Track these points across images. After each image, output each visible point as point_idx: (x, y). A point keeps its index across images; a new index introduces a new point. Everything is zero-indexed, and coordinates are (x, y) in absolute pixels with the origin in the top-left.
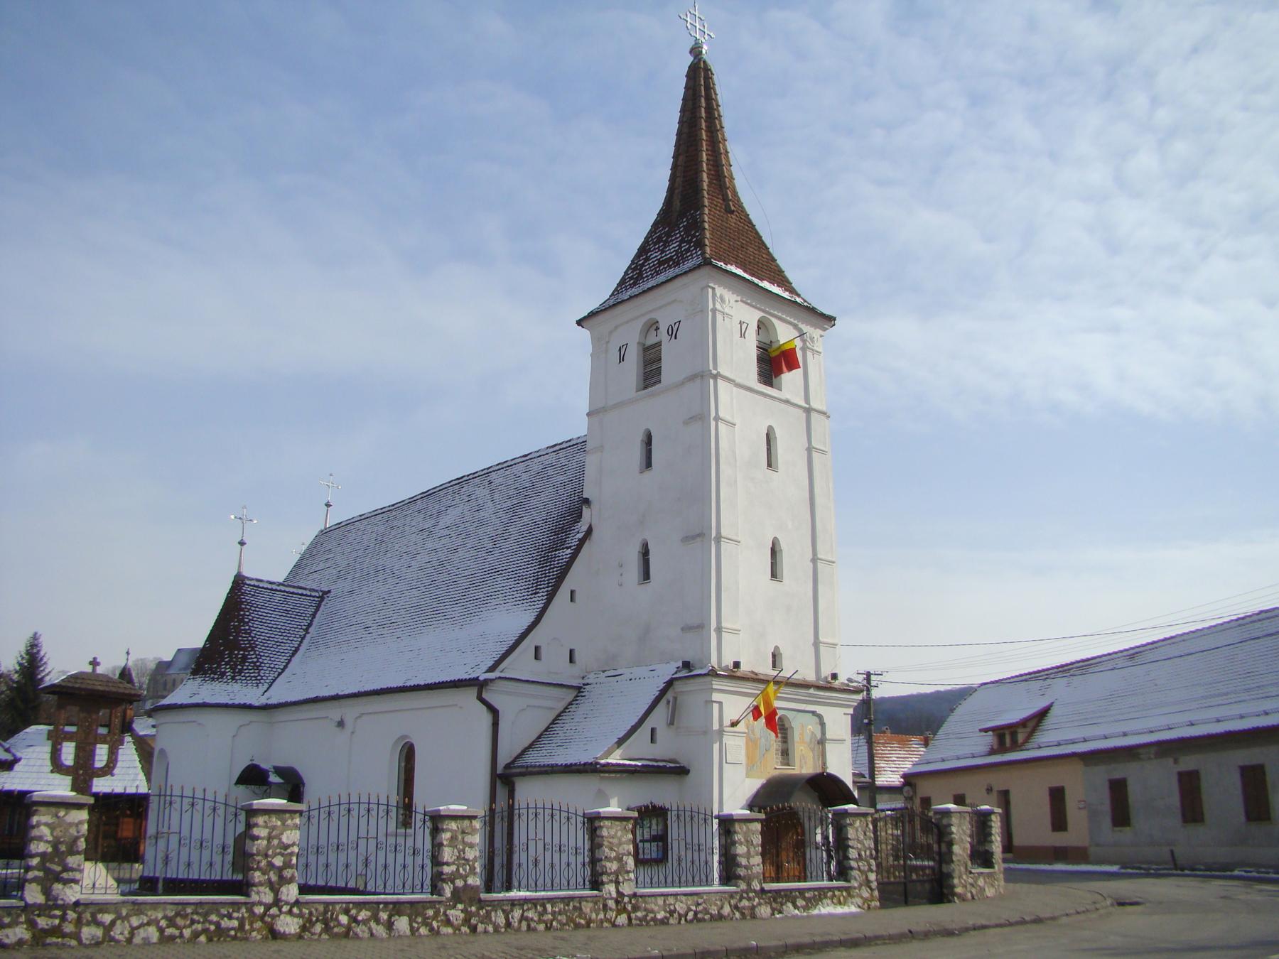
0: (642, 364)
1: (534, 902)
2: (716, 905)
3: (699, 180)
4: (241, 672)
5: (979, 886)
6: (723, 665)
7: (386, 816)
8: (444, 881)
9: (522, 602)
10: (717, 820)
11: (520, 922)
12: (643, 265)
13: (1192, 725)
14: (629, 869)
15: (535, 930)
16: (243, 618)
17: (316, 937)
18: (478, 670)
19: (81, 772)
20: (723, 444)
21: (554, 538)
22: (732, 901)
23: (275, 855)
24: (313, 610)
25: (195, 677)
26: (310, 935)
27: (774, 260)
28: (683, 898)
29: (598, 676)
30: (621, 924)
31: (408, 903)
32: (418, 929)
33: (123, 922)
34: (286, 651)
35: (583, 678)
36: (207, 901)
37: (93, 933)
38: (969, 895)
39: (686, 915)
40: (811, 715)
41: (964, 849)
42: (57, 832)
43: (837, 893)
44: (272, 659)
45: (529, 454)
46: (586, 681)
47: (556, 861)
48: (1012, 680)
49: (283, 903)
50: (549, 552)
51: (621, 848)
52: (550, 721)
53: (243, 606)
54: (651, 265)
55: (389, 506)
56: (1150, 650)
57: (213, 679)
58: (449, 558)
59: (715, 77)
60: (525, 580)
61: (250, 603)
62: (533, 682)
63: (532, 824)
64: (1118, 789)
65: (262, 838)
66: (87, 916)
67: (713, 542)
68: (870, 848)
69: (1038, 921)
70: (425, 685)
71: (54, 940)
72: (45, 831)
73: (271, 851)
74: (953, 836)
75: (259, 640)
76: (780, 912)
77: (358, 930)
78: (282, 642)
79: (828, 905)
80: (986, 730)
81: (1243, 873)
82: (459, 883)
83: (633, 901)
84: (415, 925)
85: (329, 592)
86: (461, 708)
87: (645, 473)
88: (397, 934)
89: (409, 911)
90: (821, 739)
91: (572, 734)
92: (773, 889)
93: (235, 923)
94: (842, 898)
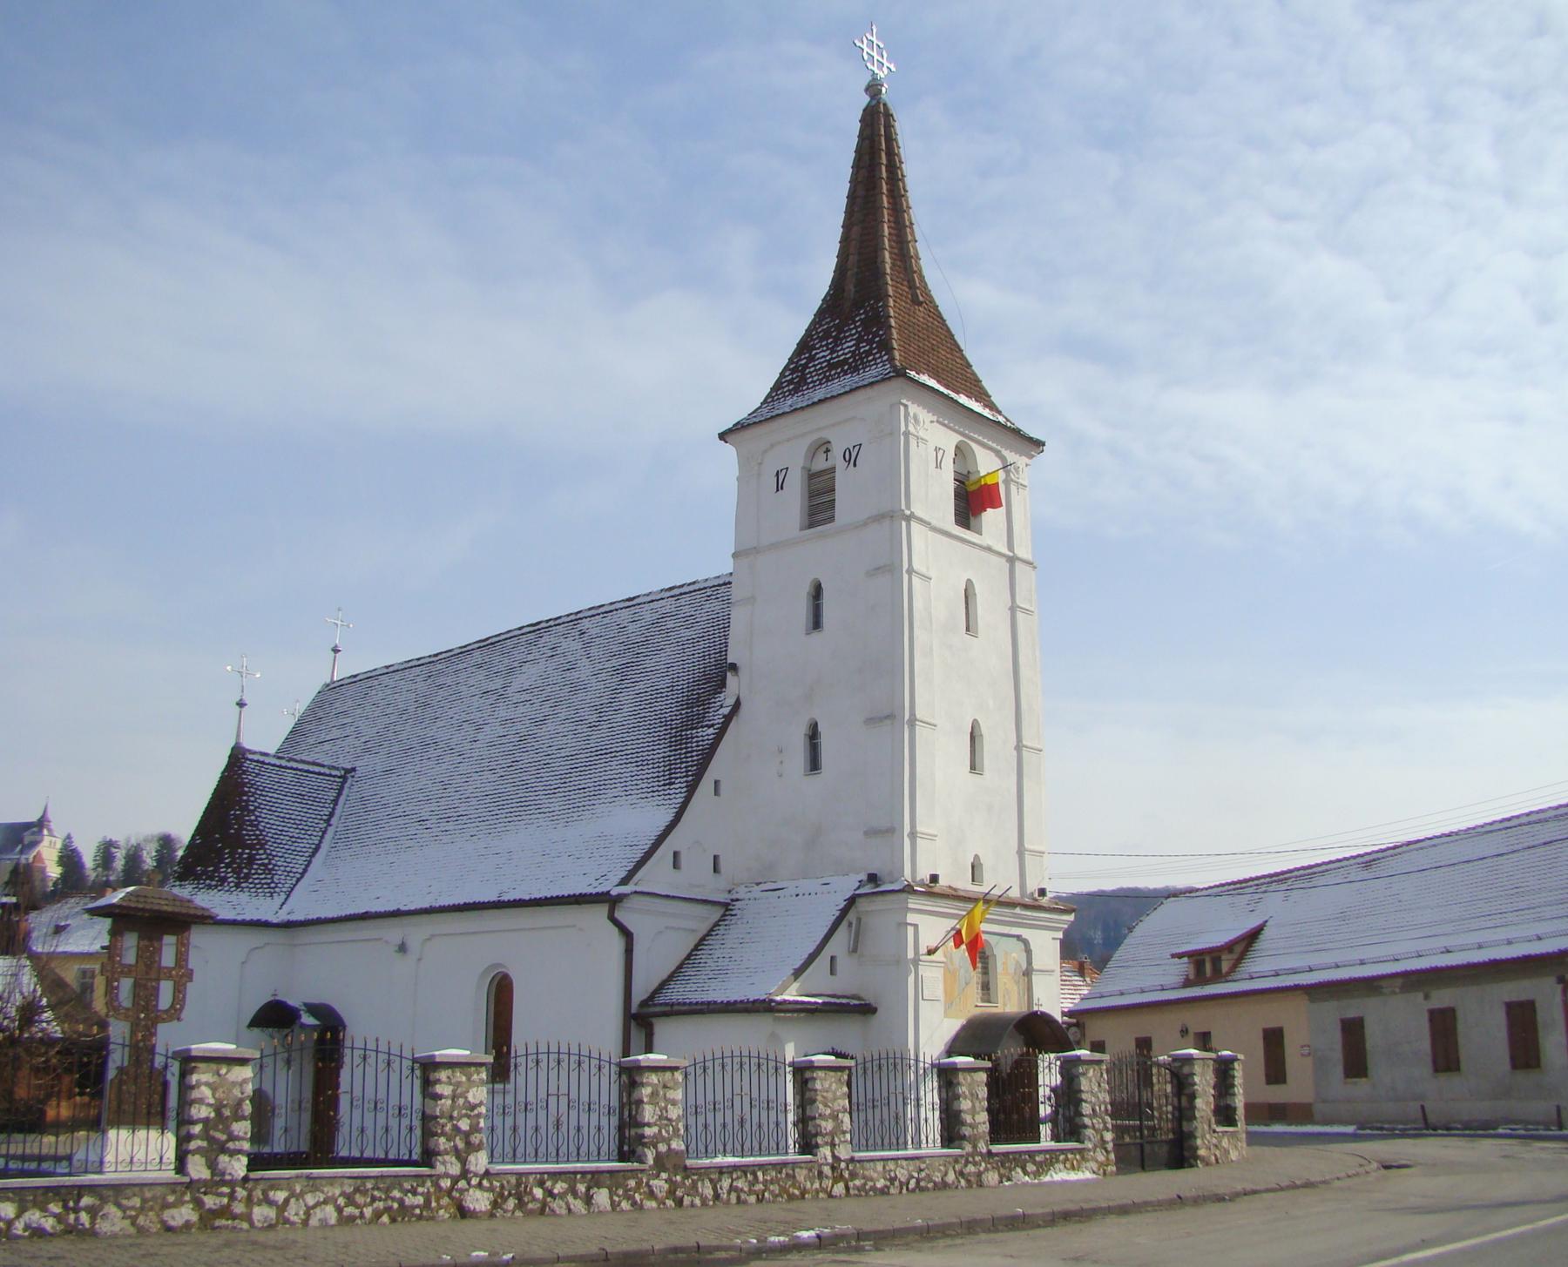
0: (807, 495)
1: (744, 1169)
2: (940, 1171)
3: (879, 260)
4: (247, 877)
6: (918, 879)
7: (557, 1068)
8: (645, 1145)
10: (791, 1068)
11: (729, 1193)
12: (806, 366)
13: (1448, 952)
14: (845, 1129)
15: (745, 1202)
16: (247, 805)
17: (509, 1214)
18: (606, 883)
19: (143, 1015)
21: (687, 713)
22: (956, 1166)
23: (461, 1117)
24: (335, 795)
25: (183, 883)
27: (969, 366)
28: (904, 1163)
29: (750, 889)
30: (838, 1195)
31: (608, 1172)
33: (297, 1200)
34: (304, 850)
35: (730, 892)
37: (265, 1213)
38: (1213, 1158)
39: (908, 1183)
40: (1015, 939)
41: (1207, 1103)
43: (1070, 1156)
46: (734, 897)
47: (584, 1123)
48: (1210, 891)
49: (472, 1175)
50: (682, 731)
51: (836, 1104)
52: (692, 946)
53: (246, 789)
54: (818, 367)
55: (430, 656)
57: (209, 887)
59: (897, 124)
61: (255, 784)
62: (674, 897)
63: (737, 1076)
64: (1353, 1031)
65: (446, 1097)
66: (258, 1193)
67: (906, 726)
68: (1104, 1102)
69: (1309, 1185)
70: (530, 900)
72: (206, 1092)
74: (1196, 1087)
75: (270, 835)
76: (1009, 1179)
77: (555, 1205)
78: (298, 838)
79: (1060, 1171)
80: (1180, 956)
81: (1509, 1131)
82: (662, 1148)
83: (850, 1168)
84: (616, 1199)
85: (354, 769)
86: (580, 929)
87: (813, 635)
88: (596, 1210)
89: (608, 1182)
90: (1027, 969)
91: (726, 963)
92: (1000, 1151)
94: (1075, 1162)
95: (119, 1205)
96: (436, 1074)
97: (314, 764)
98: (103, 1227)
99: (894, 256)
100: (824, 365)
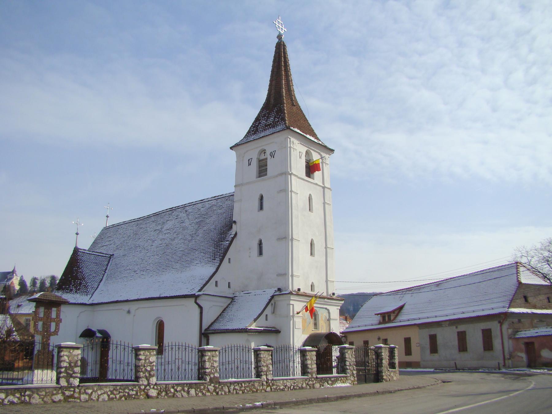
0: (258, 167)
1: (238, 383)
2: (301, 383)
3: (281, 92)
4: (79, 289)
5: (392, 376)
8: (206, 375)
9: (208, 263)
10: (253, 350)
11: (233, 390)
12: (258, 126)
13: (464, 313)
14: (270, 370)
15: (238, 393)
17: (163, 397)
19: (46, 333)
20: (294, 202)
25: (58, 291)
26: (161, 396)
27: (310, 126)
28: (289, 381)
32: (198, 393)
33: (95, 392)
34: (97, 280)
35: (234, 294)
36: (124, 384)
37: (85, 397)
39: (291, 387)
40: (325, 309)
41: (386, 362)
42: (70, 359)
43: (342, 378)
44: (92, 284)
45: (203, 200)
46: (235, 295)
47: (187, 368)
48: (387, 294)
50: (218, 242)
51: (267, 362)
53: (79, 261)
54: (262, 126)
55: (138, 219)
56: (445, 282)
57: (67, 292)
58: (171, 243)
59: (287, 48)
60: (208, 254)
61: (81, 259)
62: (216, 296)
63: (236, 353)
64: (433, 339)
65: (143, 360)
66: (83, 390)
67: (290, 241)
68: (353, 361)
69: (419, 388)
70: (170, 296)
71: (72, 400)
72: (66, 358)
73: (146, 364)
74: (383, 356)
76: (323, 386)
78: (96, 277)
79: (339, 383)
80: (377, 314)
82: (212, 376)
83: (272, 382)
84: (197, 392)
85: (113, 255)
88: (191, 396)
89: (195, 387)
90: (328, 319)
93: (134, 393)
94: (344, 380)
95: (38, 394)
96: (140, 352)
97: (100, 253)
98: (33, 401)
99: (286, 90)
100: (264, 125)
